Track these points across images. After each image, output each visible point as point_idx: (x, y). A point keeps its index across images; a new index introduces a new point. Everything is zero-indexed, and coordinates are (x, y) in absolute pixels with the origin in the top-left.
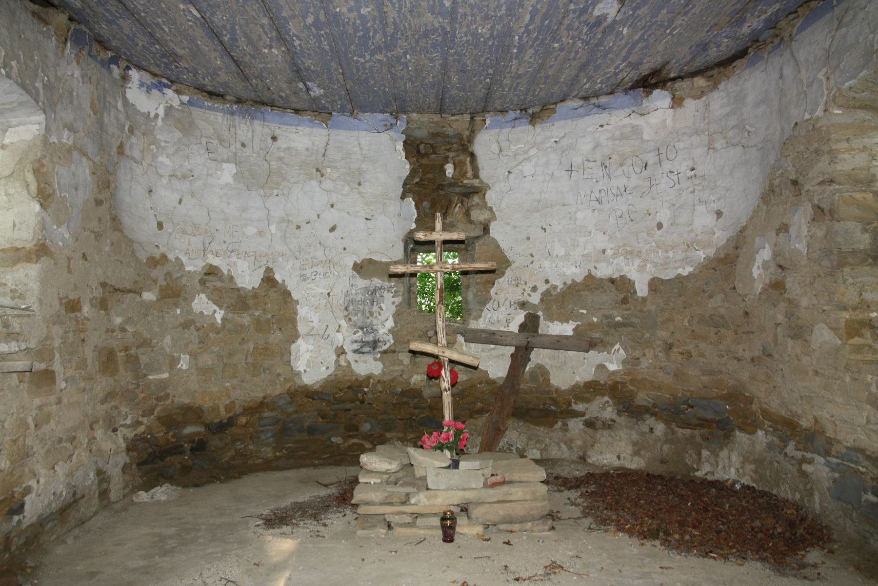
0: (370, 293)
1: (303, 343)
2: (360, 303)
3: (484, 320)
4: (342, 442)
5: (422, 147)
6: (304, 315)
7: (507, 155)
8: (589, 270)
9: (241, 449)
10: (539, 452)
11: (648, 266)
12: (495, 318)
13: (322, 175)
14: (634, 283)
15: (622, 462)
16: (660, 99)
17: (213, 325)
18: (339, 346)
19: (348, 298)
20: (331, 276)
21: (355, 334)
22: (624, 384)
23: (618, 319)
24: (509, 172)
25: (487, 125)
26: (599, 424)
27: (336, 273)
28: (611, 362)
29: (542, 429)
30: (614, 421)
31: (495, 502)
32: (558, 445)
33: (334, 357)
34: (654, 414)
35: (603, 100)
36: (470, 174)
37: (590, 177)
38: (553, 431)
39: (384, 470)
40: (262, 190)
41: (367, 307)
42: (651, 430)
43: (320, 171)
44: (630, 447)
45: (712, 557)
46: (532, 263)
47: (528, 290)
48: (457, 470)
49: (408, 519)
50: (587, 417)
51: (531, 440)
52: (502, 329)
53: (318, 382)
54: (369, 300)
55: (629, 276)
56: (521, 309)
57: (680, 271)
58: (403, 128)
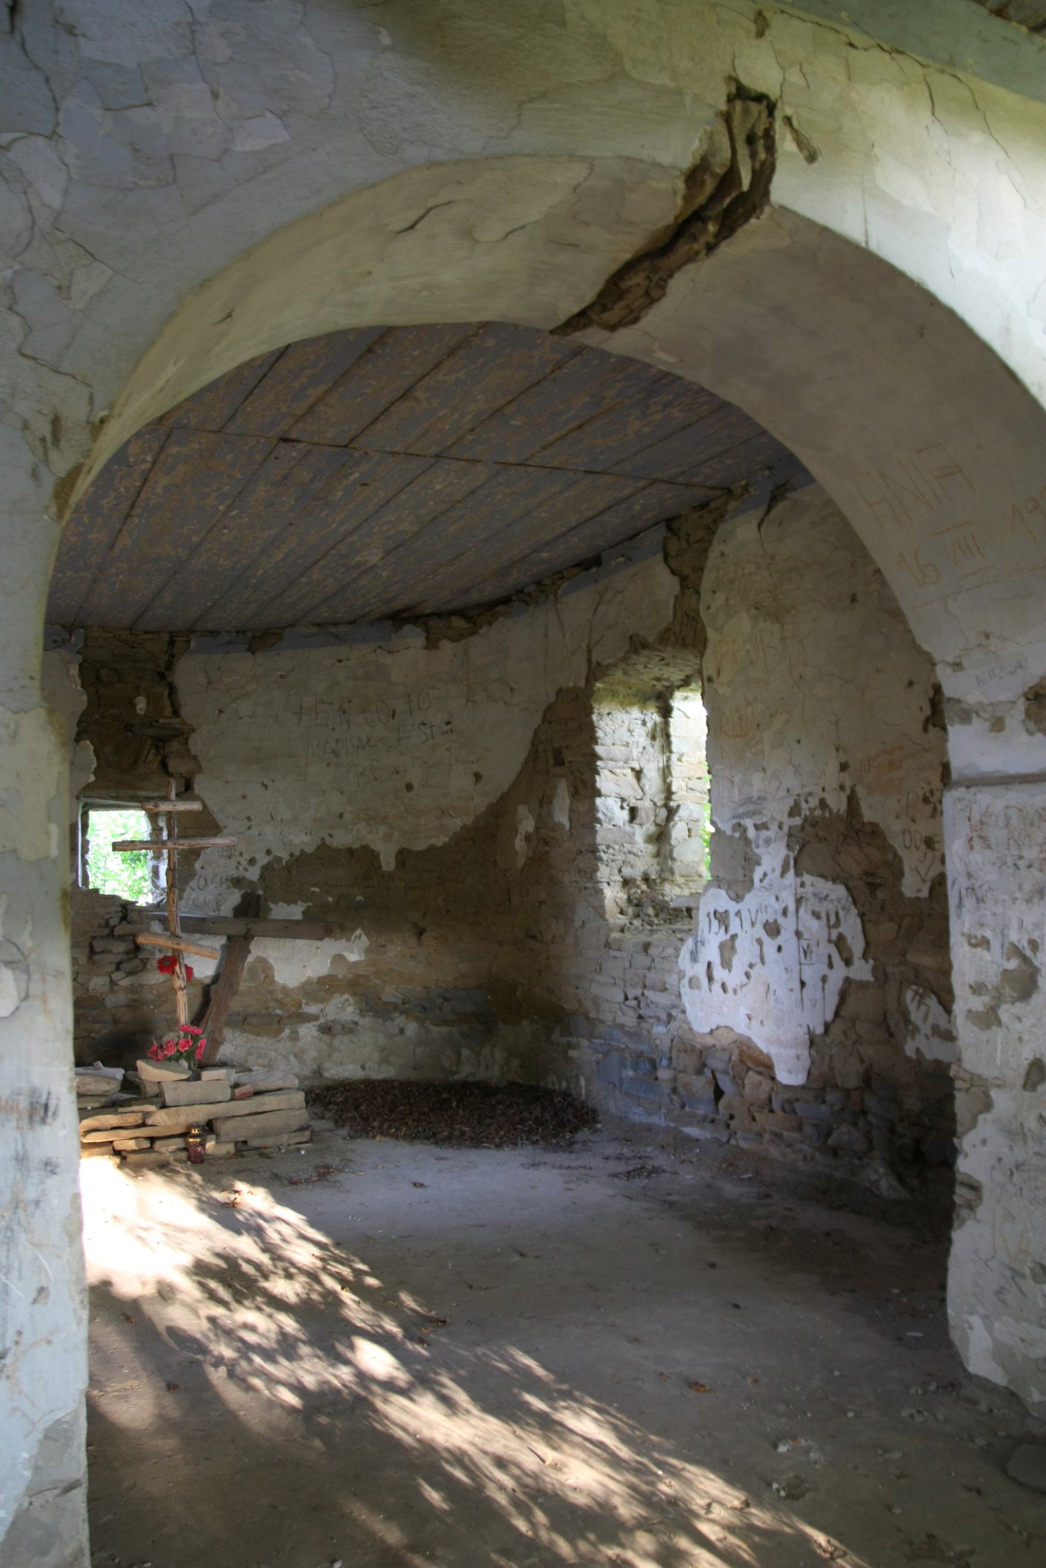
5: (104, 673)
11: (396, 834)
12: (201, 899)
14: (378, 856)
16: (413, 638)
22: (367, 977)
23: (359, 898)
24: (221, 711)
26: (337, 1028)
28: (351, 951)
29: (265, 1039)
30: (356, 1023)
31: (246, 1115)
32: (286, 1057)
34: (403, 1012)
35: (341, 629)
36: (168, 711)
38: (279, 1041)
39: (100, 1092)
42: (402, 1031)
45: (484, 1147)
46: (249, 828)
47: (244, 863)
48: (198, 1082)
50: (322, 1020)
51: (251, 1054)
52: (211, 913)
55: (372, 846)
56: (235, 887)
57: (433, 841)
58: (80, 646)
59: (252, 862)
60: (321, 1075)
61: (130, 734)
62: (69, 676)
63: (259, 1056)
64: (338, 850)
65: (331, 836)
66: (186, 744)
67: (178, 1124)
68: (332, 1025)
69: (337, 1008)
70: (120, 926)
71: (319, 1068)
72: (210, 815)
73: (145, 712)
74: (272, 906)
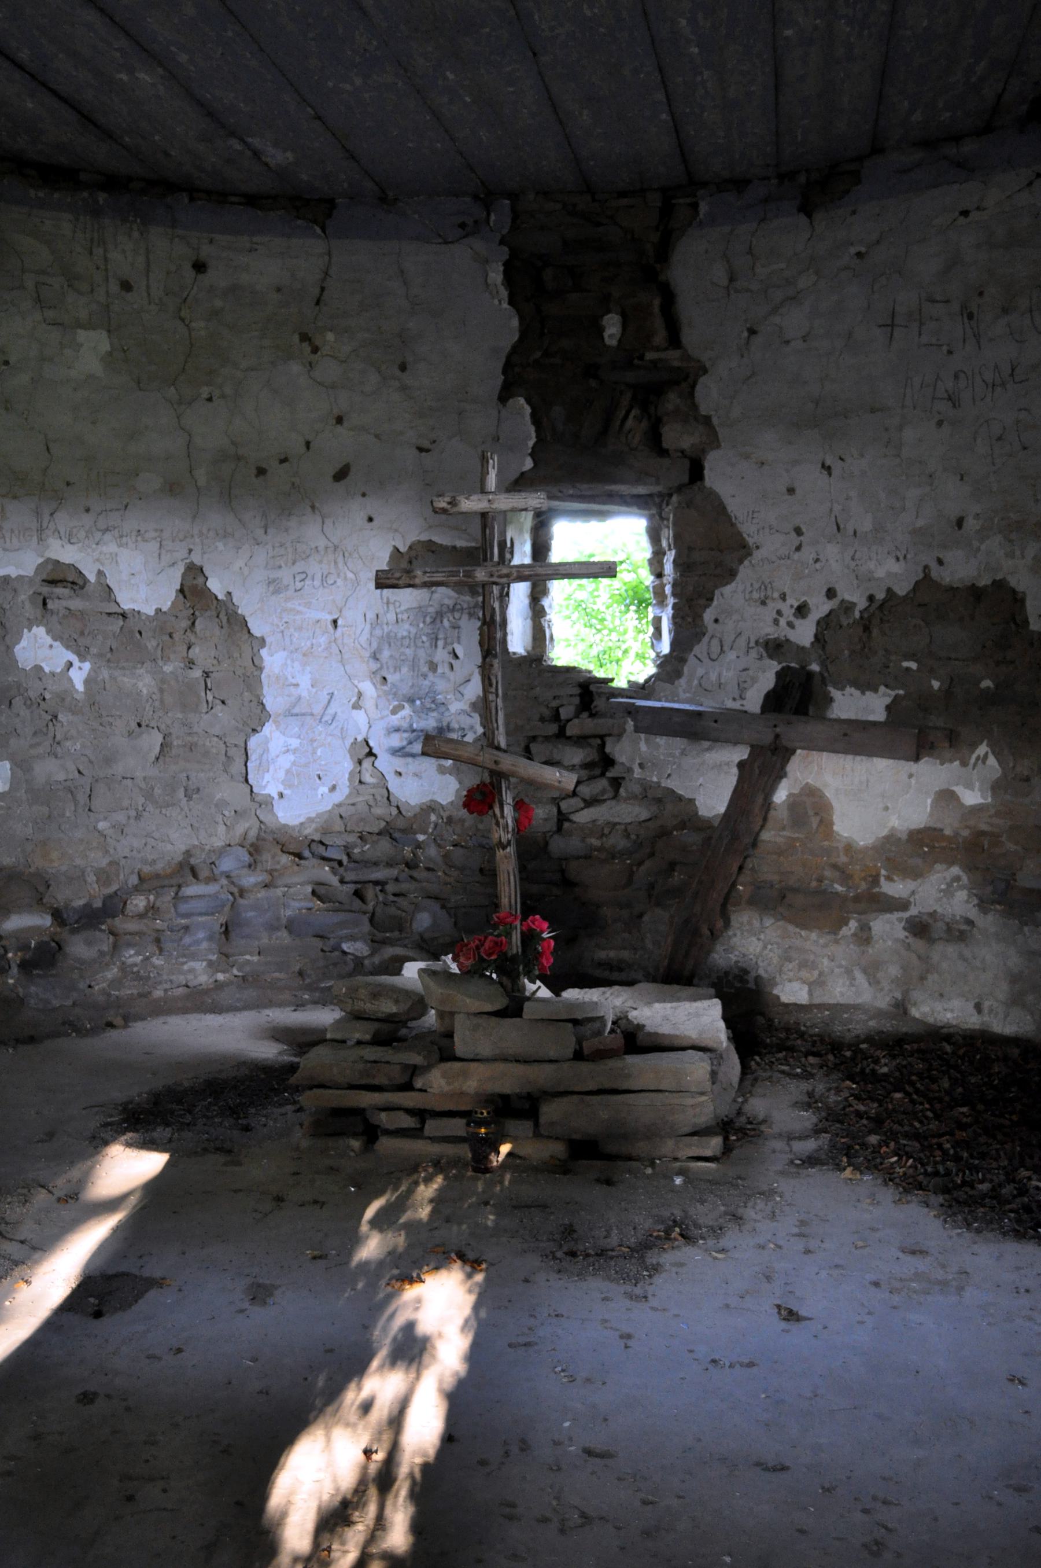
0: (428, 620)
1: (277, 734)
2: (406, 642)
3: (689, 682)
4: (366, 954)
6: (277, 671)
7: (748, 290)
8: (926, 567)
9: (136, 965)
10: (806, 988)
12: (713, 677)
13: (315, 350)
14: (1023, 601)
15: (986, 1018)
17: (65, 696)
18: (360, 738)
19: (378, 632)
20: (340, 582)
21: (394, 712)
23: (986, 683)
24: (752, 332)
25: (701, 216)
27: (350, 575)
28: (969, 786)
29: (814, 936)
30: (970, 922)
32: (849, 972)
33: (348, 765)
35: (969, 147)
36: (660, 337)
37: (934, 341)
40: (172, 388)
41: (421, 653)
43: (310, 340)
44: (1004, 986)
46: (798, 548)
47: (788, 613)
49: (407, 1122)
50: (913, 911)
51: (789, 960)
52: (730, 704)
53: (310, 820)
54: (428, 635)
55: (1013, 582)
58: (505, 231)
59: (802, 611)
60: (905, 1012)
61: (593, 383)
62: (487, 284)
63: (803, 965)
64: (952, 588)
65: (940, 562)
66: (692, 394)
67: (462, 1094)
68: (930, 921)
69: (941, 891)
70: (576, 721)
71: (903, 1000)
72: (733, 525)
73: (620, 341)
74: (835, 693)
